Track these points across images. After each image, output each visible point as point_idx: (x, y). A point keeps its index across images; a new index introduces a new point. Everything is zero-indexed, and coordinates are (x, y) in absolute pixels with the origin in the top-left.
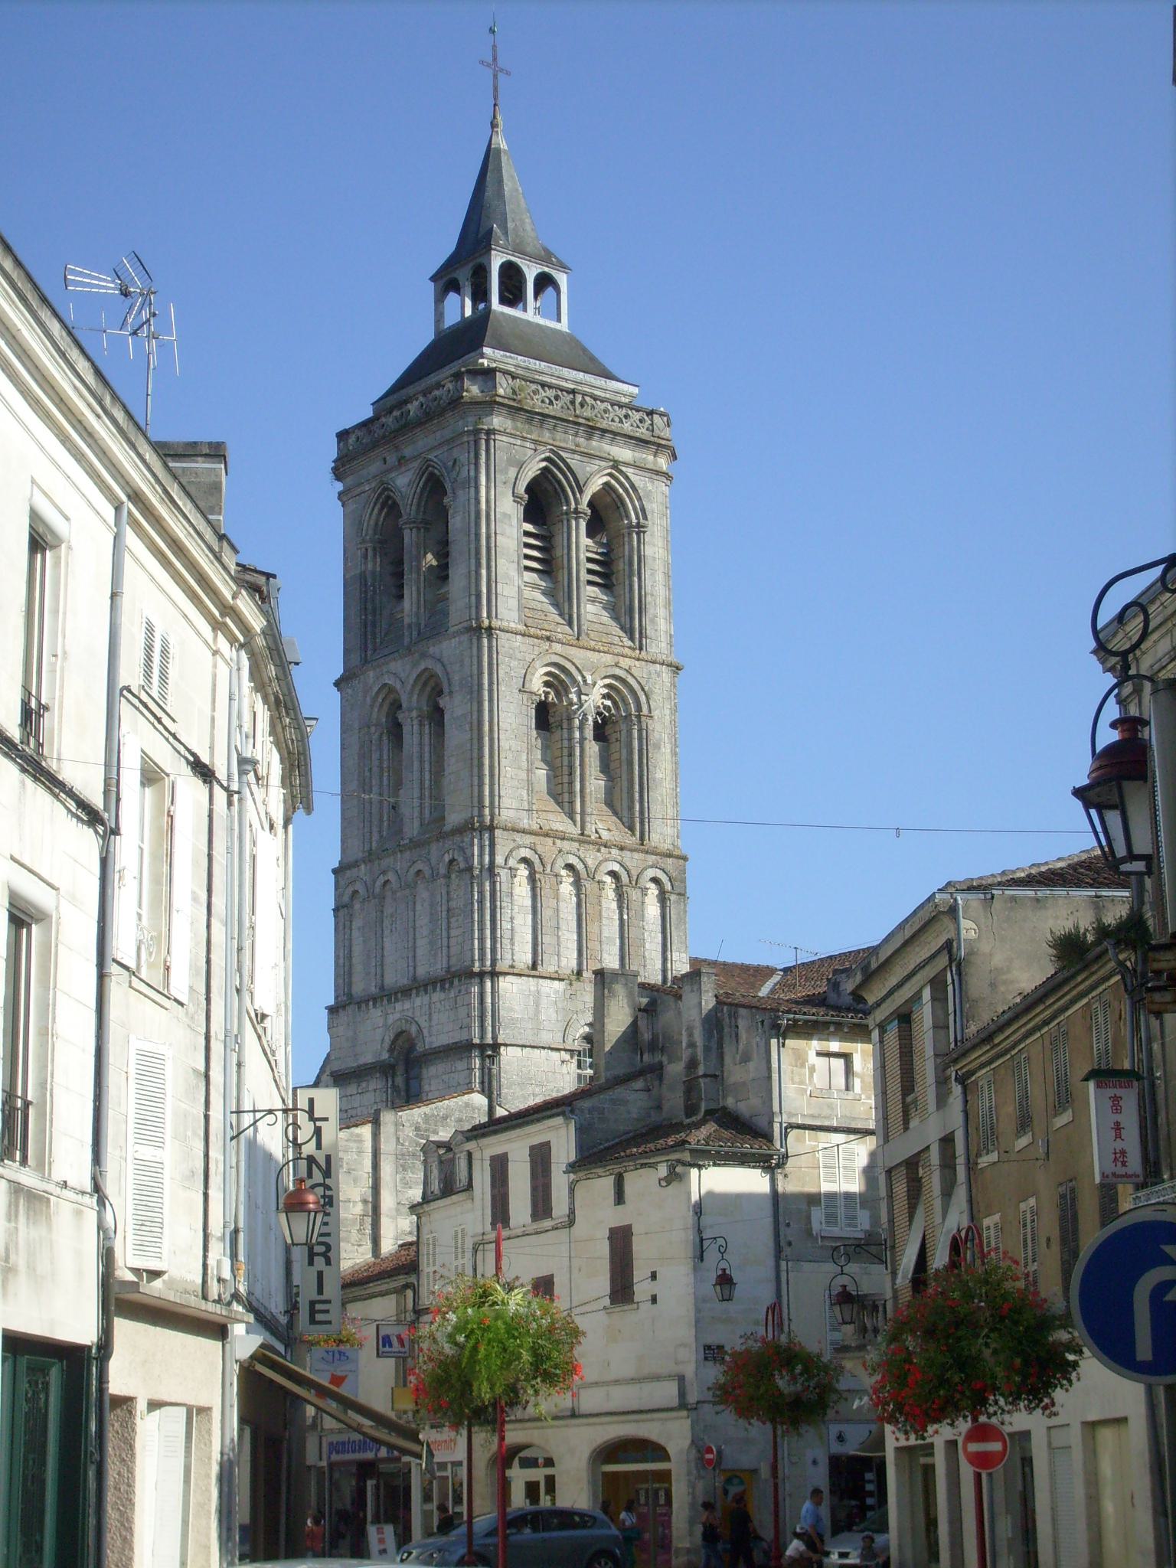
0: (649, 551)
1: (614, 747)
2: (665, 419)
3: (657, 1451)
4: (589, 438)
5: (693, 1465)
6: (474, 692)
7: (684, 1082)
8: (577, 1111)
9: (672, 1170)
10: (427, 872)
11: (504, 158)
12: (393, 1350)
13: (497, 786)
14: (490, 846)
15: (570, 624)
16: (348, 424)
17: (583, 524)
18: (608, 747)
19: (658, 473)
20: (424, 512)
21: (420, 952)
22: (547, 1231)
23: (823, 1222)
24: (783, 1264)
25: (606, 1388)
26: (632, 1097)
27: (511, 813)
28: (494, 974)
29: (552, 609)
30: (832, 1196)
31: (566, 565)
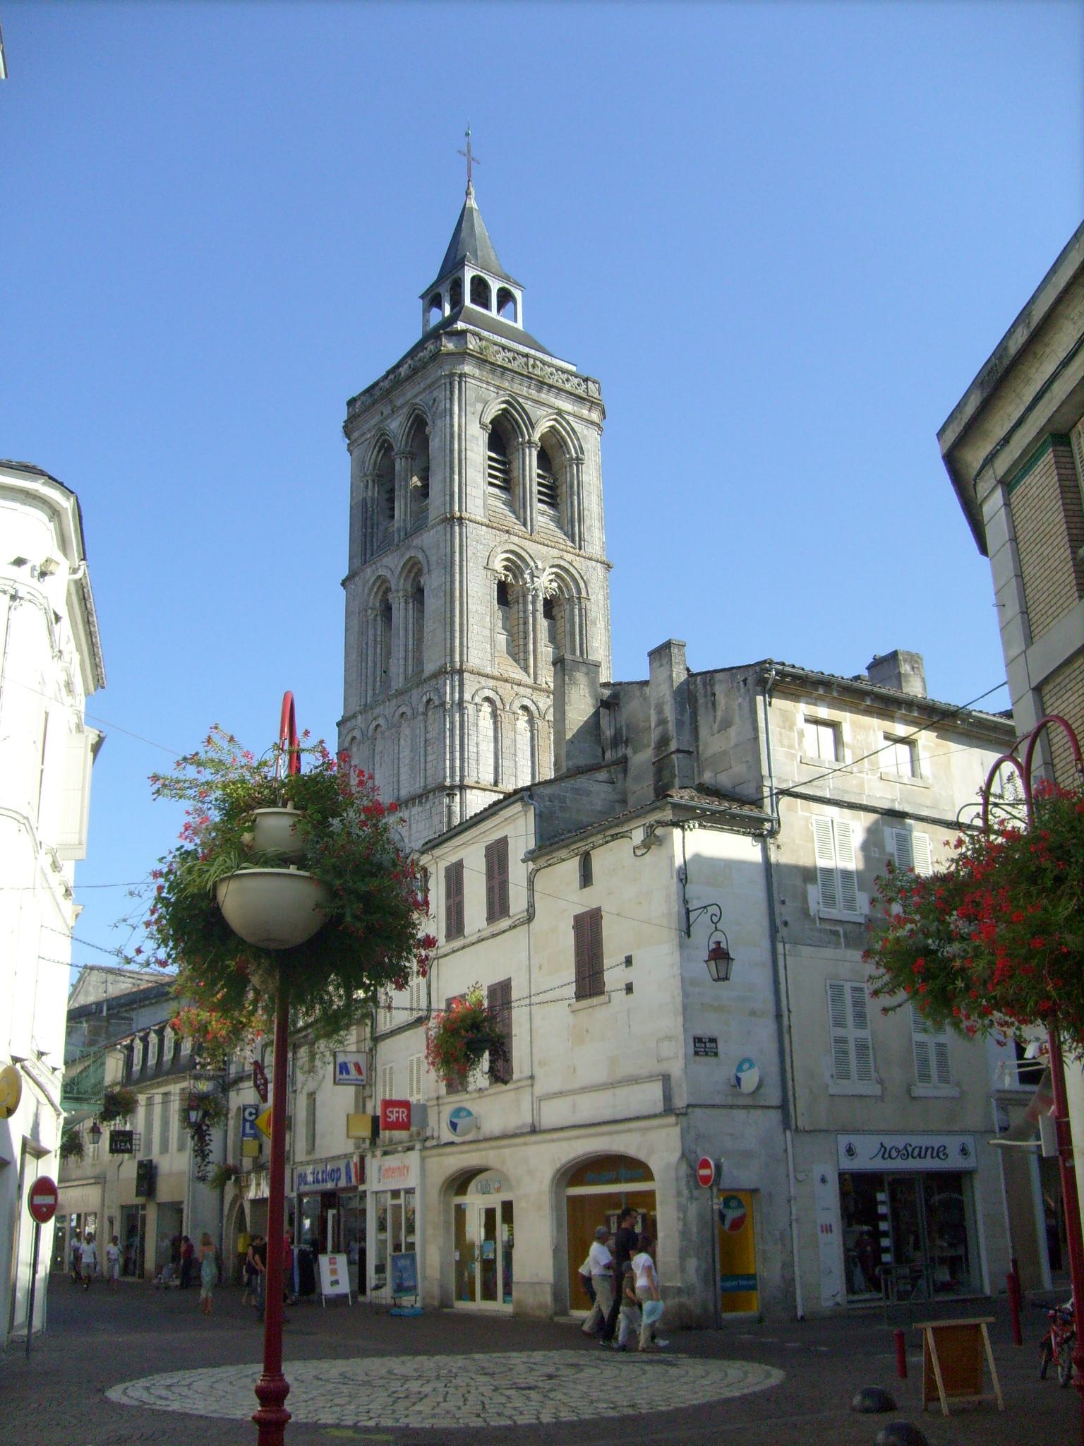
0: (585, 478)
1: (560, 623)
2: (597, 386)
3: (633, 1167)
4: (539, 391)
5: (683, 1182)
6: (448, 567)
7: (654, 763)
8: (536, 797)
9: (650, 830)
10: (409, 713)
11: (475, 214)
12: (350, 1077)
13: (465, 639)
14: (459, 686)
15: (525, 525)
16: (355, 394)
17: (535, 453)
18: (555, 623)
19: (592, 423)
20: (411, 447)
21: (403, 777)
22: (504, 932)
23: (821, 900)
24: (780, 946)
25: (572, 1097)
26: (595, 788)
27: (477, 661)
28: (462, 788)
29: (511, 514)
30: (827, 872)
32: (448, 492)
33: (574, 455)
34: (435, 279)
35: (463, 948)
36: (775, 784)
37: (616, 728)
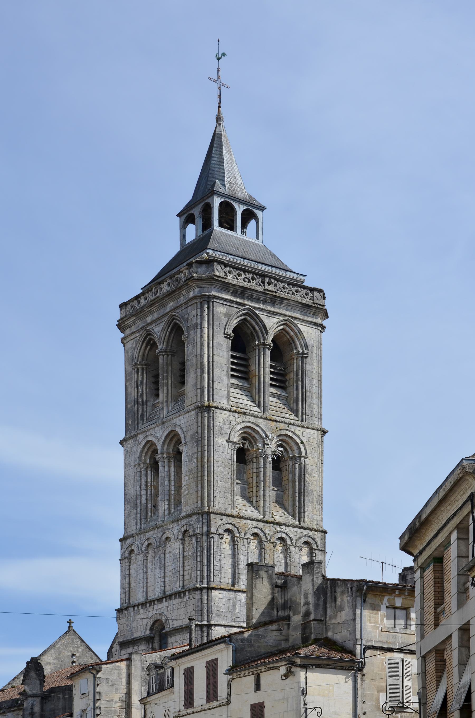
1: (285, 473)
7: (302, 624)
8: (233, 641)
15: (259, 406)
17: (268, 352)
18: (281, 474)
20: (171, 346)
22: (215, 708)
27: (221, 505)
28: (209, 589)
31: (257, 374)
32: (199, 387)
33: (300, 351)
34: (190, 197)
35: (194, 713)
36: (364, 642)
37: (285, 600)
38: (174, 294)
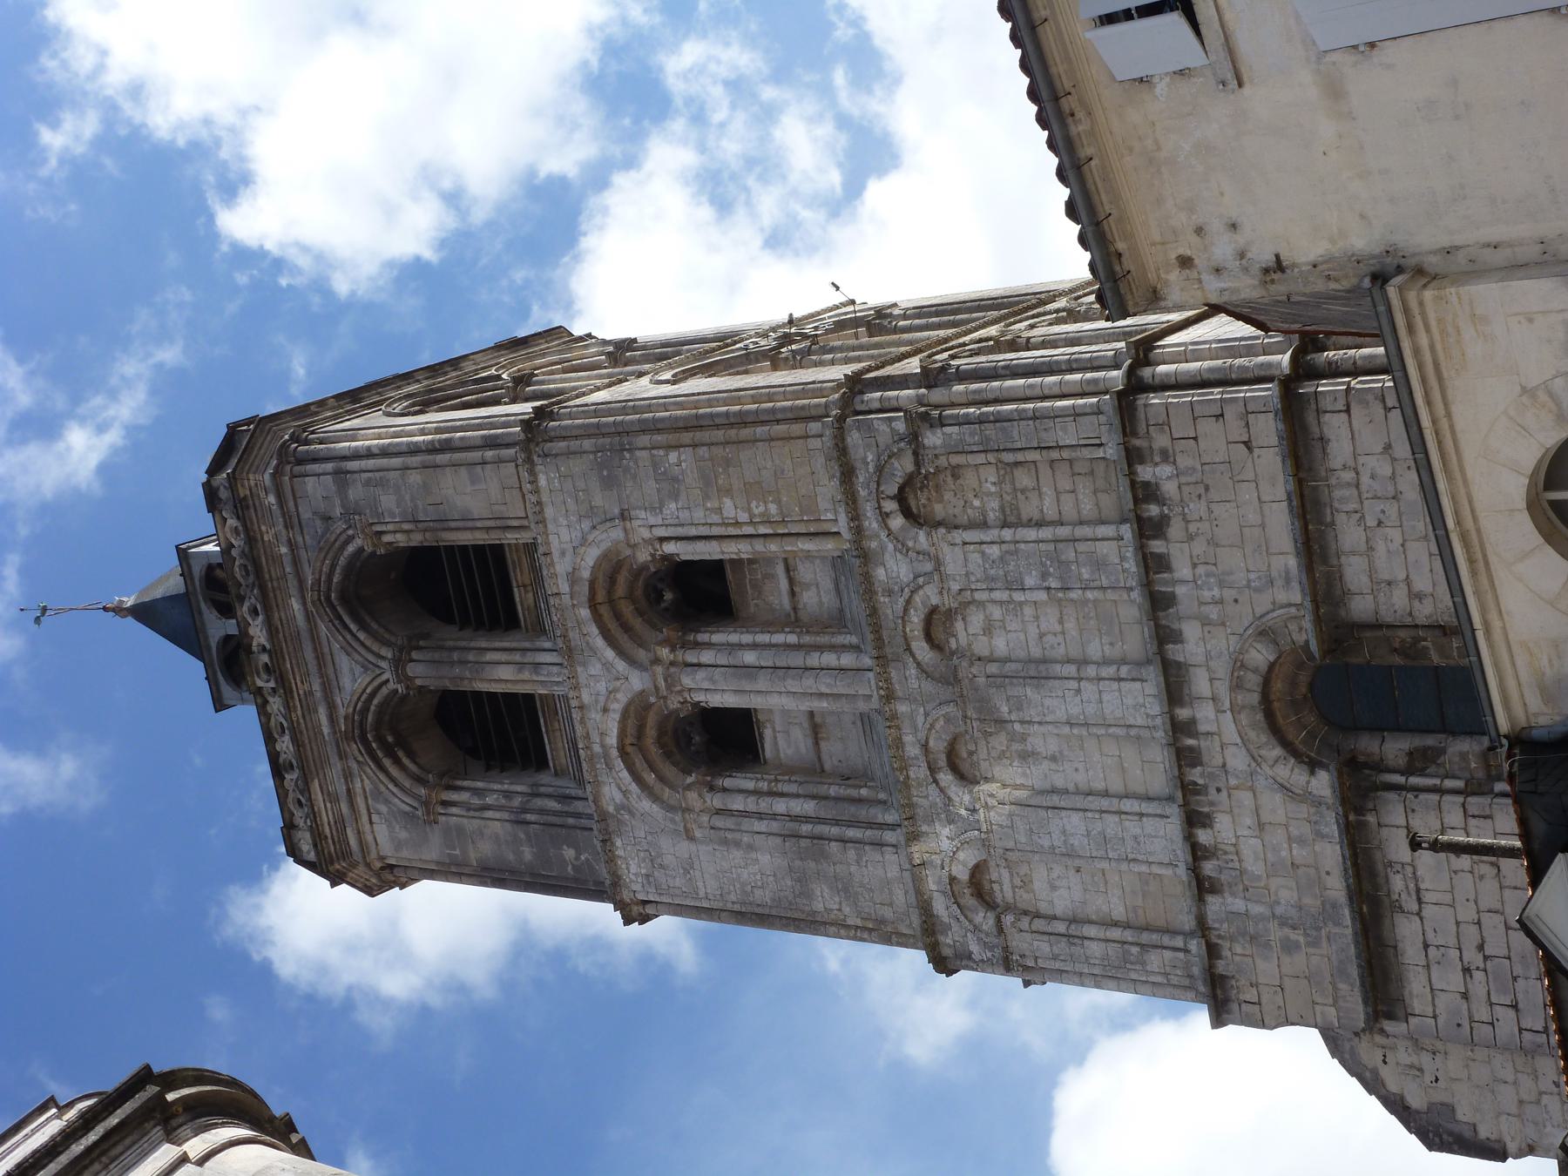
38: (267, 576)
